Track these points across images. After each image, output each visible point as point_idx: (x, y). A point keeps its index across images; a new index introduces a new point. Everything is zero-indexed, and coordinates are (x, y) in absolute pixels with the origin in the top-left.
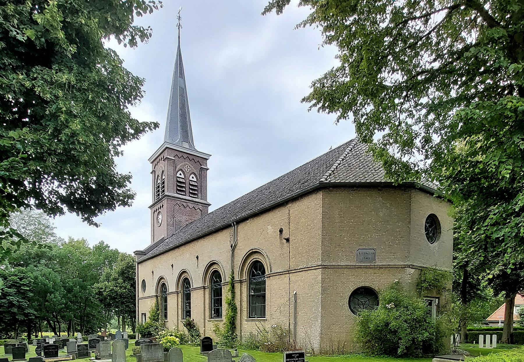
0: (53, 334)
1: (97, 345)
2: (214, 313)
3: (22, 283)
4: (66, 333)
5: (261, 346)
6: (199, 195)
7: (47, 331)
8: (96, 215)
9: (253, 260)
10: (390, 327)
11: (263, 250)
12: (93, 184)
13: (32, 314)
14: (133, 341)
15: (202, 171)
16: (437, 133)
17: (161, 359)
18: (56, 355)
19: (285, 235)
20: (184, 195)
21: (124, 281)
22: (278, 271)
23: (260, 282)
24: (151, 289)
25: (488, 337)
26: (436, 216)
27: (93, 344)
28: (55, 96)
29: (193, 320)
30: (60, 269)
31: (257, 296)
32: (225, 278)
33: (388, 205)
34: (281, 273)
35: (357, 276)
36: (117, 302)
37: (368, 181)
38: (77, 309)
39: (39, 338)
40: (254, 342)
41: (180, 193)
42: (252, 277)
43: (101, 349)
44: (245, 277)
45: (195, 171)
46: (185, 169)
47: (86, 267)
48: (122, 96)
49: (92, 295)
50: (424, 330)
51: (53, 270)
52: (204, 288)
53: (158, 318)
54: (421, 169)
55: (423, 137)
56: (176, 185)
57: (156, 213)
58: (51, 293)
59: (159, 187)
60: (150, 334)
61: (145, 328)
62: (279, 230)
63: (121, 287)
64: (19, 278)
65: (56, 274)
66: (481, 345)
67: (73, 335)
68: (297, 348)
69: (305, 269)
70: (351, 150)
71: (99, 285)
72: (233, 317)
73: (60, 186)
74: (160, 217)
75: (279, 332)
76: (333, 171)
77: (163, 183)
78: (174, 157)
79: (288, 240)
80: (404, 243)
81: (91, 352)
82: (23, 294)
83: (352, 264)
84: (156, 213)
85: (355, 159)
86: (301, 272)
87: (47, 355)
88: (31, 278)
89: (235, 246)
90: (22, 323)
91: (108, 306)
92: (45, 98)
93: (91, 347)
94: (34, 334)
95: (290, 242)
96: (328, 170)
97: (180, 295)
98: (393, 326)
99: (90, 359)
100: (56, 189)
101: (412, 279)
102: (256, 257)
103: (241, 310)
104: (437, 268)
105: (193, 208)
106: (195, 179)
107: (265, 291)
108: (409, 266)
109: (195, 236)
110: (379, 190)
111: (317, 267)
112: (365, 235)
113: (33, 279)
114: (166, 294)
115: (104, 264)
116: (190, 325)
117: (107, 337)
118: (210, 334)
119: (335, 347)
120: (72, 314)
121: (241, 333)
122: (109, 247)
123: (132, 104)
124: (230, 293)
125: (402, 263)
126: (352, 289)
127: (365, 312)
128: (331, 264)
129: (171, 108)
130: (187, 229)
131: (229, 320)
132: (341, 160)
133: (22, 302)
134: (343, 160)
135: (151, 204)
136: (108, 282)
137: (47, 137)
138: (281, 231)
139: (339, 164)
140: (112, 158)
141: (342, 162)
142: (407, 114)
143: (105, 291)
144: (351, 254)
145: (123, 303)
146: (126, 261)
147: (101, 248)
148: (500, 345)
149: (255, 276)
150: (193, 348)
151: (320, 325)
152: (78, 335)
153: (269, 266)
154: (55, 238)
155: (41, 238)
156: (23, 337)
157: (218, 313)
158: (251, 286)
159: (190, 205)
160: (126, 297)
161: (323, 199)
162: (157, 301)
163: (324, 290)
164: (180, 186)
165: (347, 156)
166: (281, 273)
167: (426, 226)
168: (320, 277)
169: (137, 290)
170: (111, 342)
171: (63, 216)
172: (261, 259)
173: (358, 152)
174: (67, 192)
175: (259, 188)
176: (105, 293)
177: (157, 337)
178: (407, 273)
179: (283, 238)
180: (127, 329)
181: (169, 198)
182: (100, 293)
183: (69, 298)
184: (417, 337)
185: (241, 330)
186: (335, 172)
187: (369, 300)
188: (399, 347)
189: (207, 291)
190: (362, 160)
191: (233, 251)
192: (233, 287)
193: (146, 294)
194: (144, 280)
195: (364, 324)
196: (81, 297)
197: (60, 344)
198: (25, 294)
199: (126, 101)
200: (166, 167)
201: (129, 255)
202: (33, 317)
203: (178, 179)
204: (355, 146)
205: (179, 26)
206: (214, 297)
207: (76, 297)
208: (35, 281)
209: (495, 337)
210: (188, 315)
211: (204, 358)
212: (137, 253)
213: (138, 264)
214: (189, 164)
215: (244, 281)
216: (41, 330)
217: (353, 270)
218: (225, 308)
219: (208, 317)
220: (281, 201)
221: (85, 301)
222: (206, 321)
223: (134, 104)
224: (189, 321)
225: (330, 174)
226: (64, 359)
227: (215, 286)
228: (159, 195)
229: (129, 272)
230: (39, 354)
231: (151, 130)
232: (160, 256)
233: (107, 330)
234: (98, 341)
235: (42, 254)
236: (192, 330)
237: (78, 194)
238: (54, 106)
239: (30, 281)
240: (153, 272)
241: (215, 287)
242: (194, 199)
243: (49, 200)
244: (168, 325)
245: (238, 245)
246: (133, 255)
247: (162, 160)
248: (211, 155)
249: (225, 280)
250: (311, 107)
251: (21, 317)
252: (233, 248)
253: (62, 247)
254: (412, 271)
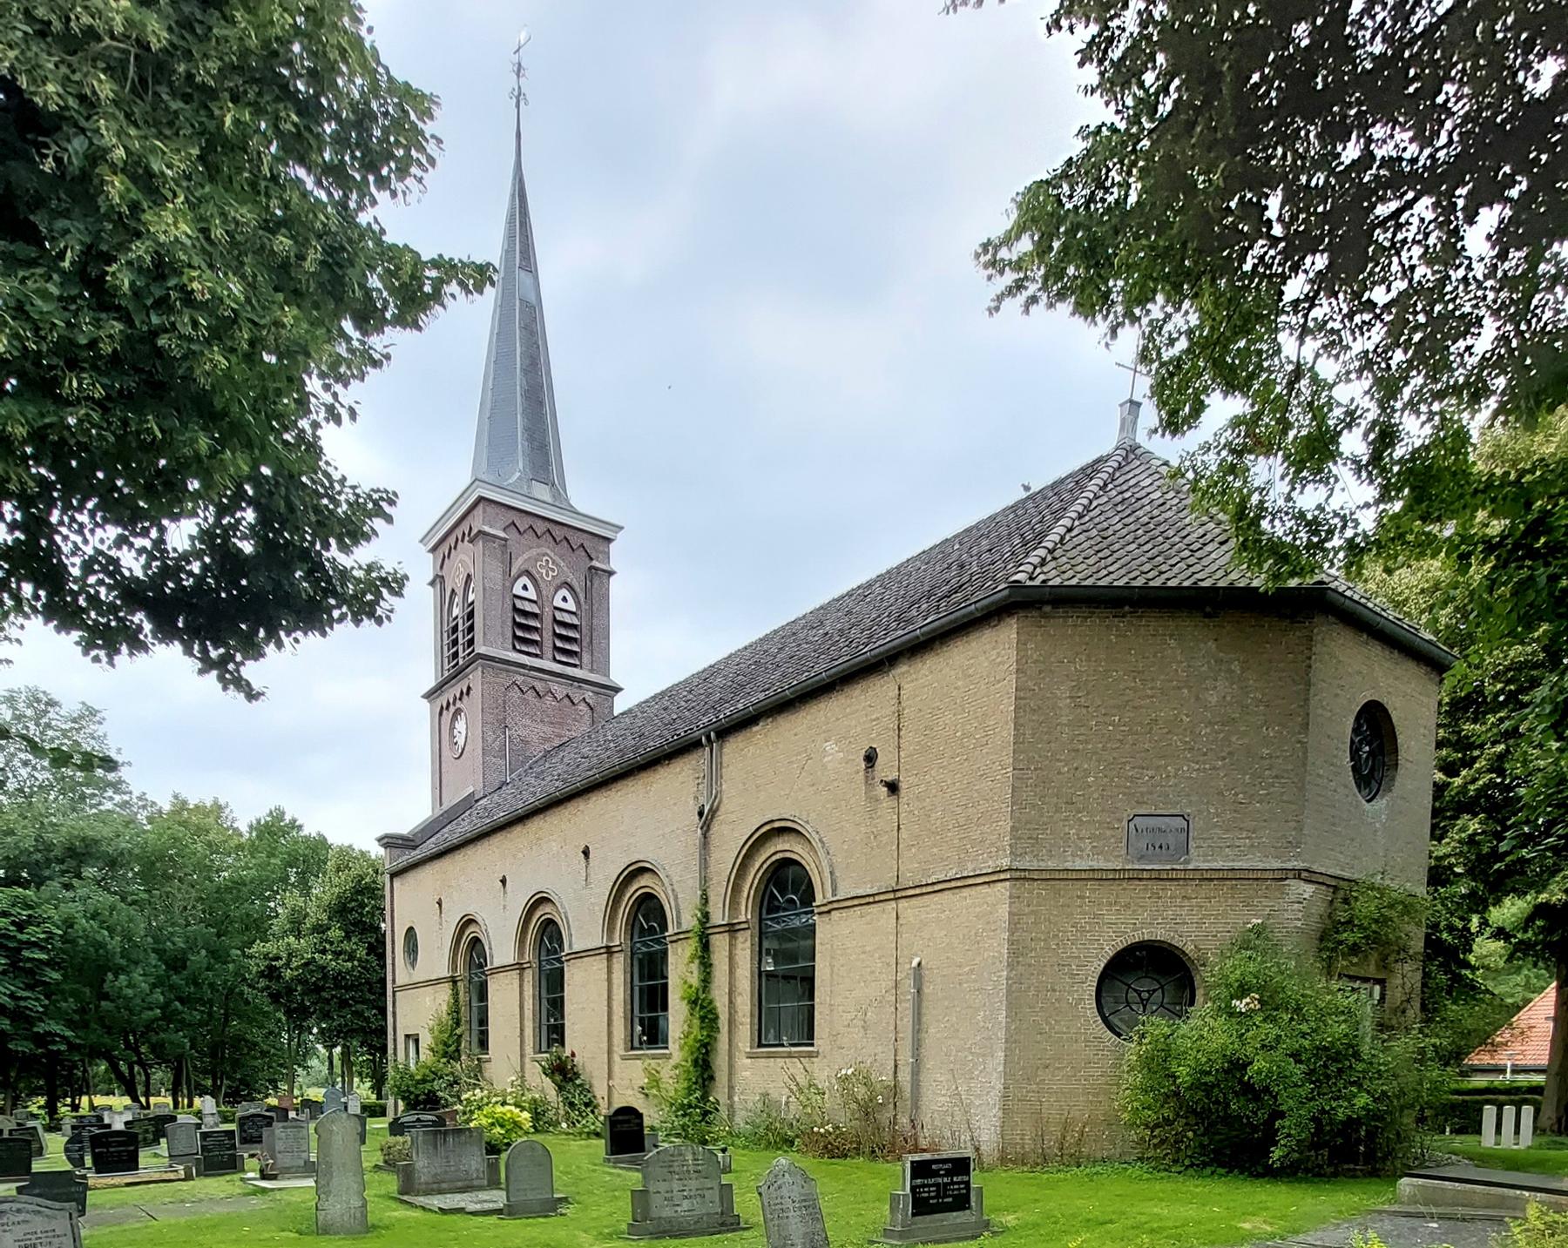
0: (127, 1100)
1: (265, 1132)
2: (643, 1033)
3: (24, 937)
4: (169, 1100)
5: (797, 1136)
6: (586, 657)
7: (110, 1093)
8: (255, 652)
9: (774, 858)
10: (1250, 1078)
11: (807, 822)
12: (244, 537)
13: (58, 1035)
14: (378, 1124)
15: (598, 576)
16: (1418, 413)
17: (478, 1178)
18: (131, 1163)
19: (886, 769)
20: (536, 656)
21: (347, 933)
22: (861, 892)
23: (794, 931)
24: (436, 958)
25: (1509, 1111)
26: (1385, 711)
27: (253, 1129)
28: (82, 98)
29: (573, 1055)
30: (146, 896)
31: (785, 978)
32: (678, 917)
33: (1236, 667)
34: (867, 900)
35: (1127, 906)
36: (327, 1001)
37: (1170, 584)
38: (201, 1024)
39: (82, 1112)
40: (778, 1125)
41: (524, 648)
42: (768, 913)
43: (279, 1146)
44: (745, 913)
45: (571, 579)
47: (228, 890)
48: (353, 157)
49: (245, 979)
50: (1353, 1084)
51: (123, 899)
52: (609, 951)
53: (457, 1050)
54: (1366, 536)
55: (1374, 423)
56: (509, 623)
57: (447, 716)
58: (118, 971)
59: (455, 629)
60: (432, 1101)
61: (418, 1082)
62: (863, 753)
63: (337, 954)
64: (13, 923)
65: (132, 911)
66: (1488, 1139)
67: (190, 1105)
68: (923, 1144)
69: (953, 884)
70: (1106, 485)
71: (270, 947)
72: (705, 1045)
73: (121, 541)
74: (461, 726)
75: (861, 1092)
76: (1051, 551)
77: (471, 615)
78: (504, 530)
79: (893, 787)
80: (1285, 798)
81: (246, 1155)
82: (30, 973)
83: (1110, 866)
84: (447, 716)
85: (1121, 515)
86: (939, 894)
87: (102, 1166)
88: (54, 924)
89: (714, 812)
90: (27, 1064)
91: (298, 1016)
92: (37, 99)
93: (244, 1141)
94: (69, 1100)
95: (903, 792)
96: (1035, 549)
97: (529, 975)
98: (1259, 1072)
99: (242, 1179)
100: (113, 553)
101: (1307, 916)
103: (731, 1022)
104: (1388, 882)
105: (566, 701)
106: (571, 606)
107: (813, 959)
108: (1298, 874)
109: (578, 781)
110: (1207, 616)
111: (995, 878)
112: (1158, 768)
113: (58, 928)
114: (483, 973)
115: (285, 879)
116: (563, 1073)
117: (297, 1110)
118: (627, 1097)
119: (1051, 1143)
120: (185, 1037)
121: (730, 1097)
122: (300, 827)
123: (394, 194)
124: (695, 966)
125: (1277, 865)
126: (1109, 952)
127: (1157, 1025)
128: (1043, 865)
129: (495, 371)
130: (547, 765)
131: (692, 1053)
132: (1074, 515)
133: (26, 999)
134: (1081, 516)
135: (431, 683)
136: (298, 937)
137: (54, 290)
138: (871, 758)
139: (1070, 530)
140: (314, 435)
141: (1077, 523)
142: (1319, 343)
143: (287, 965)
144: (1109, 833)
145: (343, 1004)
146: (353, 872)
147: (274, 830)
148: (1544, 1139)
149: (777, 912)
150: (576, 1145)
151: (1001, 1068)
152: (206, 1104)
153: (827, 874)
154: (126, 798)
155: (83, 797)
156: (34, 1109)
157: (651, 1034)
158: (766, 945)
159: (555, 687)
160: (353, 985)
161: (1021, 644)
162: (456, 995)
163: (1017, 952)
164: (523, 627)
165: (1095, 503)
166: (867, 900)
167: (1352, 742)
168: (1003, 911)
169: (389, 961)
170: (312, 1126)
171: (141, 657)
172: (800, 851)
173: (1127, 495)
174: (147, 566)
175: (783, 628)
176: (288, 974)
177: (459, 1107)
178: (1293, 898)
179: (877, 780)
180: (358, 1087)
181: (490, 666)
182: (271, 973)
183: (172, 987)
184: (1333, 1109)
185: (731, 1088)
186: (1057, 553)
187: (1162, 987)
188: (1275, 1143)
189: (619, 962)
190: (1145, 519)
191: (706, 828)
192: (705, 946)
193: (420, 974)
194: (411, 929)
195: (1158, 1063)
196: (212, 985)
197: (147, 1131)
198: (35, 974)
199: (371, 178)
200: (479, 560)
201: (362, 853)
202: (63, 1048)
203: (519, 604)
204: (1117, 474)
205: (519, 97)
206: (641, 980)
207: (196, 984)
208: (65, 933)
209: (1528, 1111)
210: (556, 1041)
211: (619, 1175)
212: (389, 842)
213: (393, 875)
214: (552, 555)
215: (745, 926)
216: (88, 1087)
217: (1115, 887)
218: (678, 1018)
219: (622, 1046)
220: (875, 656)
221: (227, 998)
222: (616, 1058)
223: (400, 195)
224: (560, 1058)
225: (1044, 559)
226: (156, 1177)
227: (644, 944)
228: (456, 655)
229: (362, 906)
230: (79, 1163)
231: (468, 292)
232: (463, 851)
233: (296, 1092)
234: (269, 1121)
235: (86, 846)
236: (569, 1086)
237: (190, 574)
238: (78, 144)
239: (51, 933)
240: (440, 903)
241: (644, 949)
242: (569, 671)
243: (88, 593)
244: (491, 1070)
245: (722, 809)
246: (377, 851)
247: (467, 538)
248: (622, 528)
249: (679, 924)
250: (1000, 298)
251: (22, 1047)
252: (707, 817)
253: (149, 827)
254: (1309, 889)
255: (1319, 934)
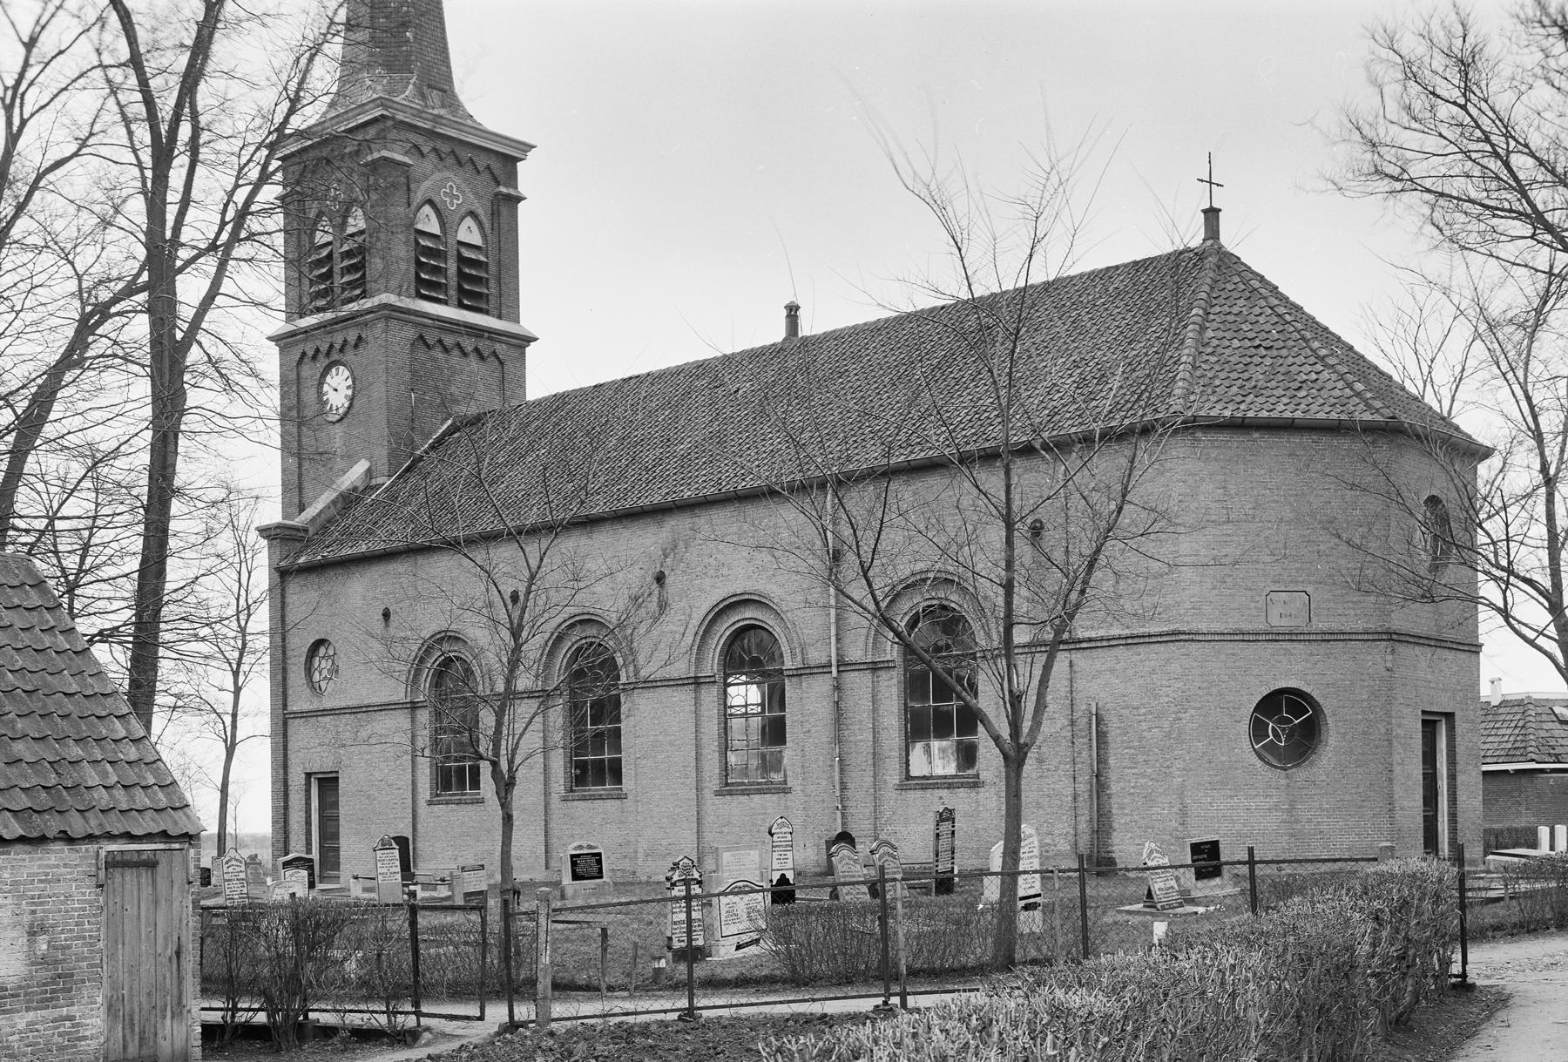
45: (480, 212)
46: (441, 198)
52: (414, 707)
102: (749, 614)
203: (467, 253)
255: (1501, 1015)
